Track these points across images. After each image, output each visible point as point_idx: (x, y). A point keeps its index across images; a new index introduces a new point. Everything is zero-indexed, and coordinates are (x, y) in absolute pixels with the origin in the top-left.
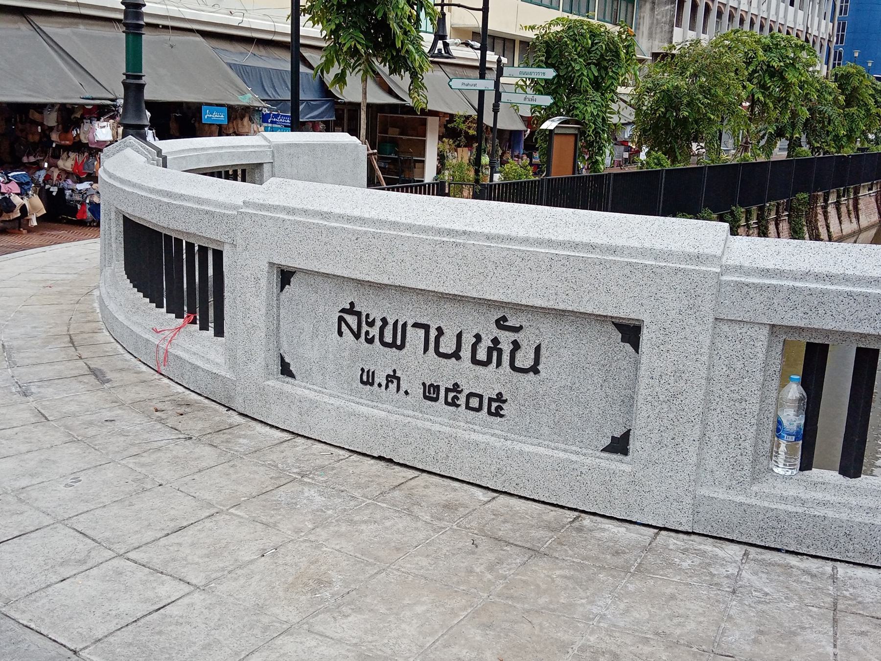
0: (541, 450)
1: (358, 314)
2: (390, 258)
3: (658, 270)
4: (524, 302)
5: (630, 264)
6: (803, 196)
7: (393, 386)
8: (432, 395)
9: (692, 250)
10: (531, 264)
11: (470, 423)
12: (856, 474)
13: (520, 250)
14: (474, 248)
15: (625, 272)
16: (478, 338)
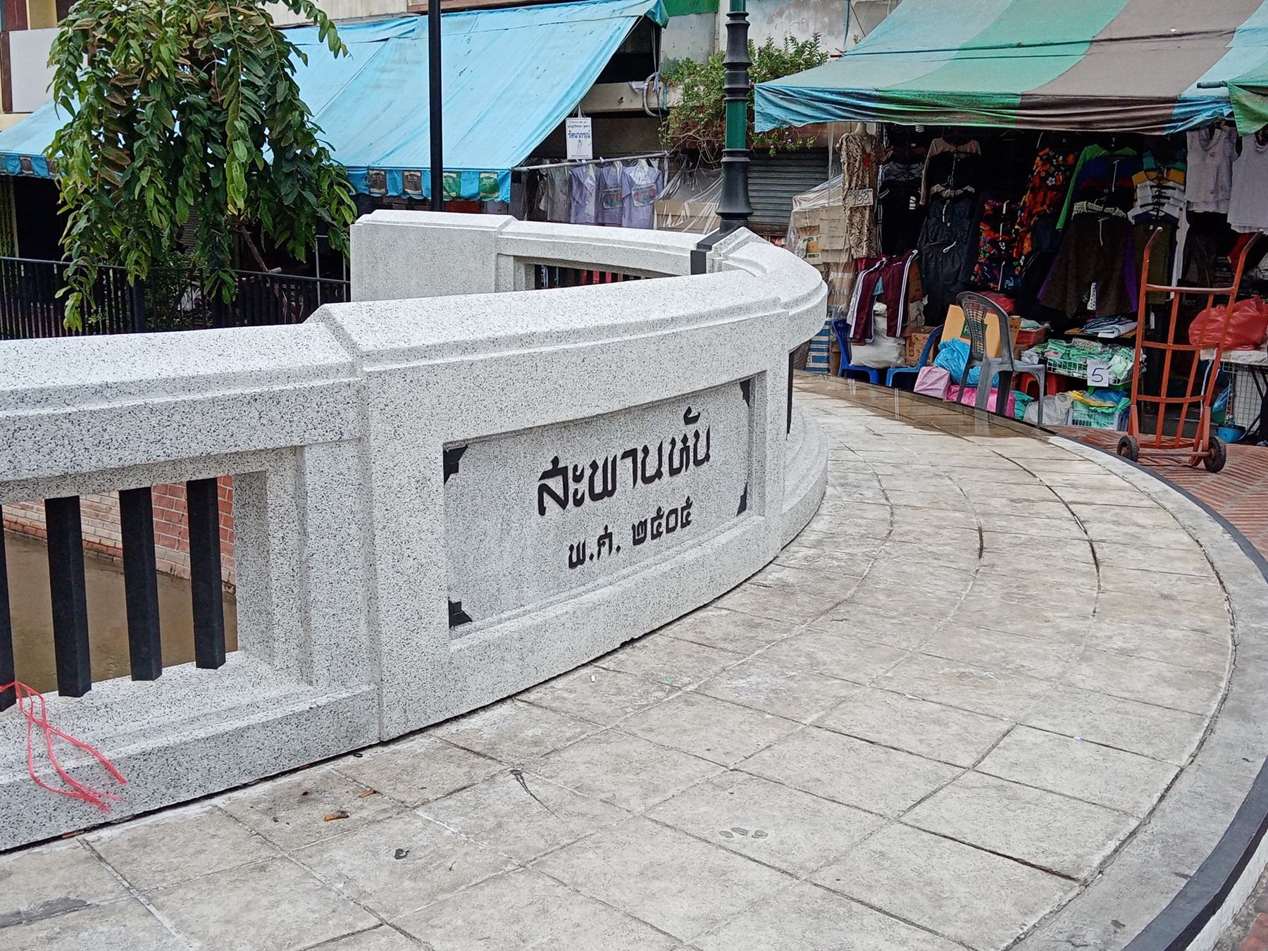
12: (77, 693)
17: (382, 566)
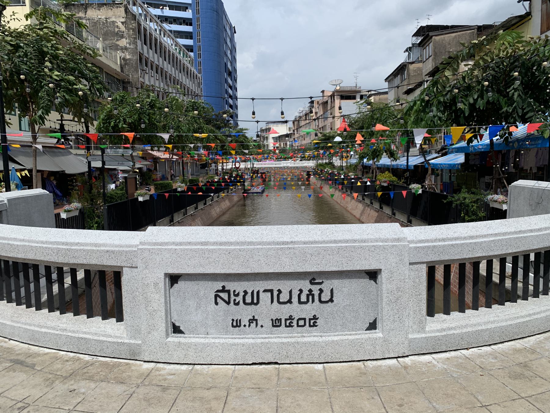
1: (228, 292)
2: (251, 260)
3: (385, 247)
5: (374, 246)
10: (329, 252)
13: (323, 247)
16: (301, 291)
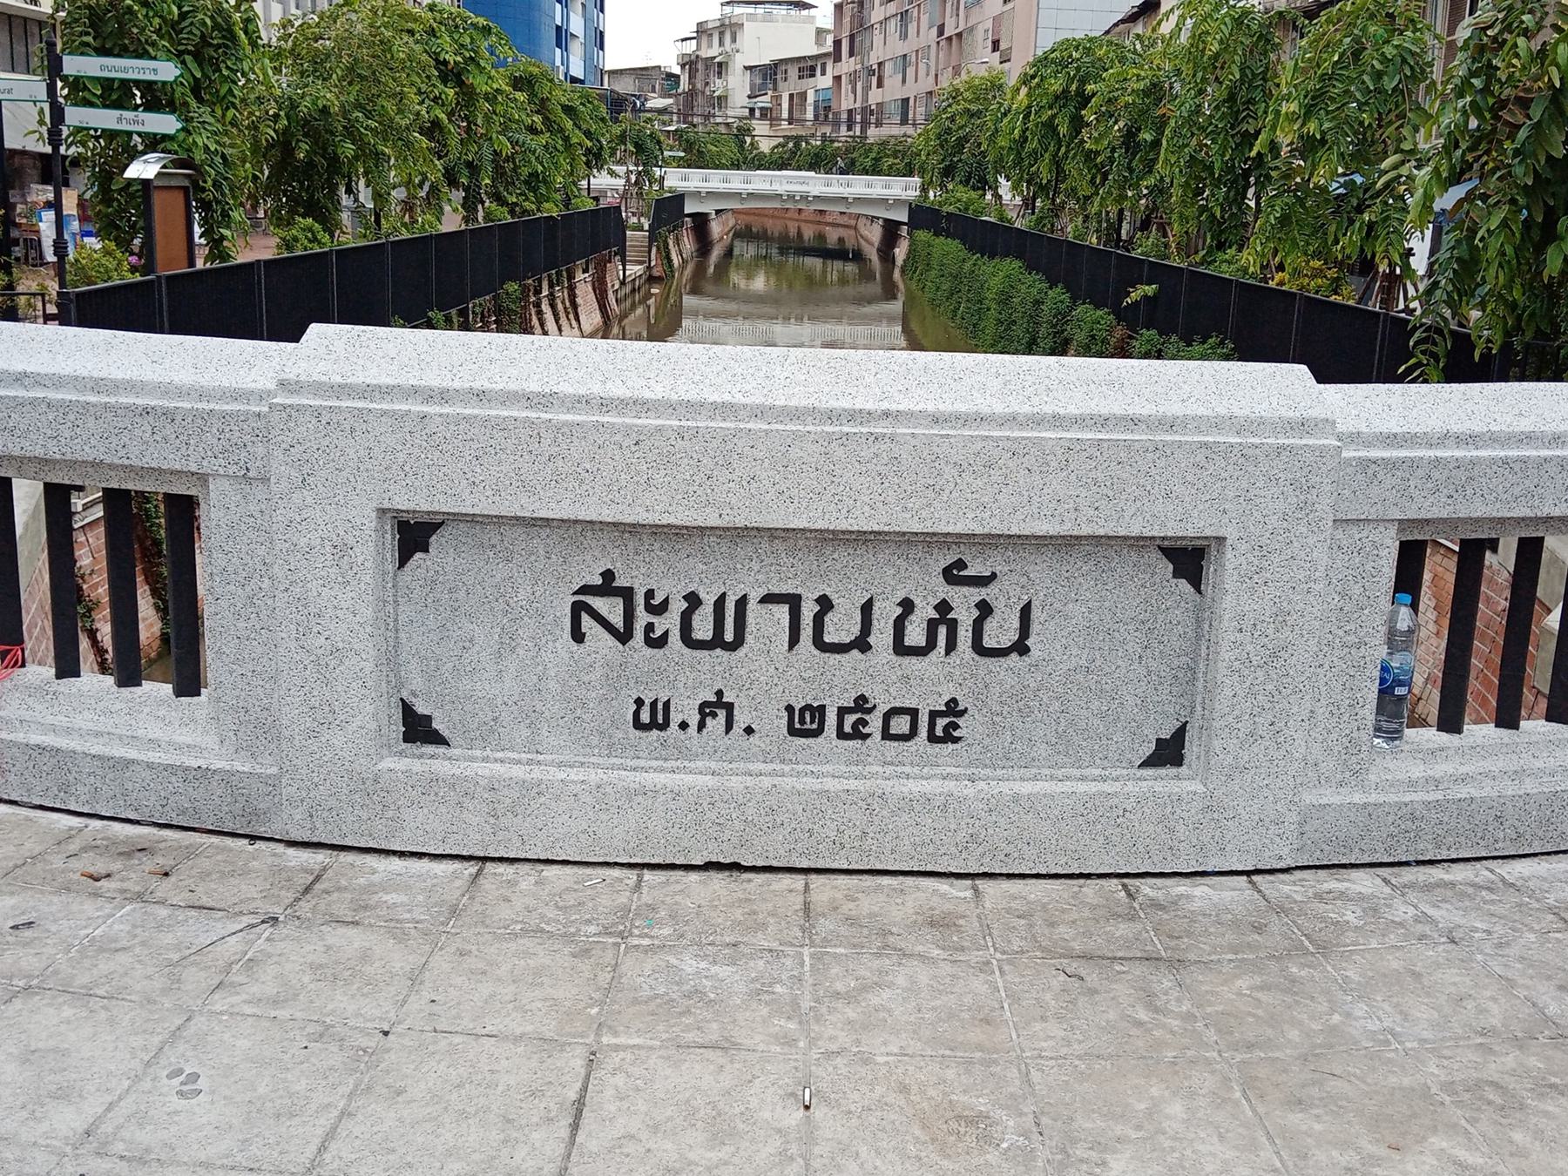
0: (1039, 787)
1: (627, 594)
4: (1015, 531)
5: (1205, 445)
6: (512, 287)
7: (716, 724)
8: (808, 726)
9: (1291, 414)
10: (1029, 461)
11: (891, 764)
13: (1008, 438)
14: (913, 442)
15: (1197, 460)
16: (907, 606)
17: (284, 635)
